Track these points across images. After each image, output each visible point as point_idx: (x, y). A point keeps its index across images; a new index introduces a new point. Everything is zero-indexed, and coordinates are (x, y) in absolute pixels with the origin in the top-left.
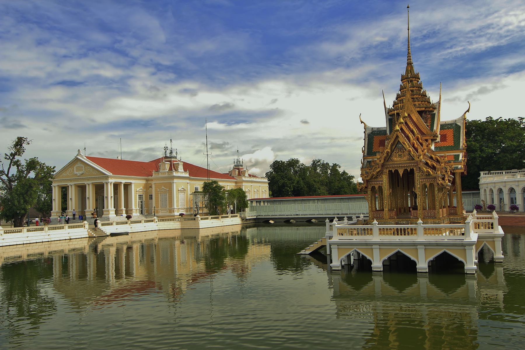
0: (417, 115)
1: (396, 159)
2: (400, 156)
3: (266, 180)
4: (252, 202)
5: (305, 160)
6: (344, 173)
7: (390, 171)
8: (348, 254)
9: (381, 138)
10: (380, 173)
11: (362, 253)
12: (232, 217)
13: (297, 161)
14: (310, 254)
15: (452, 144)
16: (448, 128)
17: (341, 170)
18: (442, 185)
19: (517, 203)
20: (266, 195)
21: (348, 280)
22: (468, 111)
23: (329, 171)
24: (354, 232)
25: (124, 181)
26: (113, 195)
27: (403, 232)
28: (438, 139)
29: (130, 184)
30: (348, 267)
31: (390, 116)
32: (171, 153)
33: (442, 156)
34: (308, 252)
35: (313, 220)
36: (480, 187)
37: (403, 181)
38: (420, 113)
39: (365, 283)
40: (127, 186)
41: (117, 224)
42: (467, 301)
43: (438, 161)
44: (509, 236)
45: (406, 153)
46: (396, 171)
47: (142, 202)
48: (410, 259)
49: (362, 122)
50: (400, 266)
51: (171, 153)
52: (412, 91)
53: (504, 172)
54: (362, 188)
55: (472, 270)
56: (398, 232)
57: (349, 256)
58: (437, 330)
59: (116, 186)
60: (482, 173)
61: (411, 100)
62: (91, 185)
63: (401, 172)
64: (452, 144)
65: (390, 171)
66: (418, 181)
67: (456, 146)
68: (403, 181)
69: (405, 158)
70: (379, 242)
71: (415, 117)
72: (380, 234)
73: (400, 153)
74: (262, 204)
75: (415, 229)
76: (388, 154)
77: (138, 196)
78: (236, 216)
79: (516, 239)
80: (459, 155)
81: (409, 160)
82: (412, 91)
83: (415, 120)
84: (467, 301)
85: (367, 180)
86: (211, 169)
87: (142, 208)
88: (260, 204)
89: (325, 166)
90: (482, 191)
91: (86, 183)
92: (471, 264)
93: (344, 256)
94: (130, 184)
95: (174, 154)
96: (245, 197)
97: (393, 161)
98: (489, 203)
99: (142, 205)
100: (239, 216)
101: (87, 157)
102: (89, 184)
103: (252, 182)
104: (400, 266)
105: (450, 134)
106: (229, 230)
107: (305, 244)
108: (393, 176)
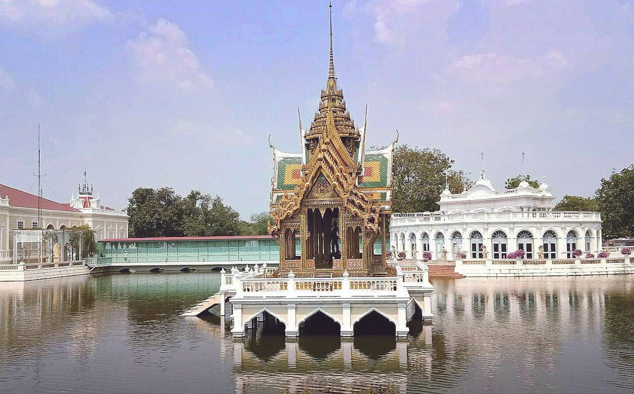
0: (340, 141)
3: (125, 214)
7: (310, 211)
8: (253, 316)
14: (198, 316)
15: (286, 182)
16: (374, 160)
18: (371, 229)
20: (126, 236)
21: (252, 347)
22: (396, 142)
24: (255, 285)
30: (252, 328)
31: (307, 140)
34: (197, 312)
37: (323, 225)
38: (343, 139)
39: (275, 352)
42: (394, 368)
45: (330, 188)
46: (317, 211)
48: (387, 320)
49: (271, 147)
50: (320, 330)
53: (416, 214)
54: (274, 231)
55: (402, 332)
57: (254, 320)
61: (333, 123)
65: (310, 211)
66: (343, 224)
68: (323, 225)
70: (293, 298)
71: (338, 143)
72: (352, 287)
74: (119, 247)
76: (308, 188)
80: (385, 193)
82: (334, 112)
83: (337, 146)
84: (394, 368)
85: (281, 220)
88: (116, 247)
92: (401, 327)
93: (249, 318)
98: (401, 250)
103: (106, 216)
104: (320, 330)
105: (375, 166)
107: (192, 300)
108: (313, 216)
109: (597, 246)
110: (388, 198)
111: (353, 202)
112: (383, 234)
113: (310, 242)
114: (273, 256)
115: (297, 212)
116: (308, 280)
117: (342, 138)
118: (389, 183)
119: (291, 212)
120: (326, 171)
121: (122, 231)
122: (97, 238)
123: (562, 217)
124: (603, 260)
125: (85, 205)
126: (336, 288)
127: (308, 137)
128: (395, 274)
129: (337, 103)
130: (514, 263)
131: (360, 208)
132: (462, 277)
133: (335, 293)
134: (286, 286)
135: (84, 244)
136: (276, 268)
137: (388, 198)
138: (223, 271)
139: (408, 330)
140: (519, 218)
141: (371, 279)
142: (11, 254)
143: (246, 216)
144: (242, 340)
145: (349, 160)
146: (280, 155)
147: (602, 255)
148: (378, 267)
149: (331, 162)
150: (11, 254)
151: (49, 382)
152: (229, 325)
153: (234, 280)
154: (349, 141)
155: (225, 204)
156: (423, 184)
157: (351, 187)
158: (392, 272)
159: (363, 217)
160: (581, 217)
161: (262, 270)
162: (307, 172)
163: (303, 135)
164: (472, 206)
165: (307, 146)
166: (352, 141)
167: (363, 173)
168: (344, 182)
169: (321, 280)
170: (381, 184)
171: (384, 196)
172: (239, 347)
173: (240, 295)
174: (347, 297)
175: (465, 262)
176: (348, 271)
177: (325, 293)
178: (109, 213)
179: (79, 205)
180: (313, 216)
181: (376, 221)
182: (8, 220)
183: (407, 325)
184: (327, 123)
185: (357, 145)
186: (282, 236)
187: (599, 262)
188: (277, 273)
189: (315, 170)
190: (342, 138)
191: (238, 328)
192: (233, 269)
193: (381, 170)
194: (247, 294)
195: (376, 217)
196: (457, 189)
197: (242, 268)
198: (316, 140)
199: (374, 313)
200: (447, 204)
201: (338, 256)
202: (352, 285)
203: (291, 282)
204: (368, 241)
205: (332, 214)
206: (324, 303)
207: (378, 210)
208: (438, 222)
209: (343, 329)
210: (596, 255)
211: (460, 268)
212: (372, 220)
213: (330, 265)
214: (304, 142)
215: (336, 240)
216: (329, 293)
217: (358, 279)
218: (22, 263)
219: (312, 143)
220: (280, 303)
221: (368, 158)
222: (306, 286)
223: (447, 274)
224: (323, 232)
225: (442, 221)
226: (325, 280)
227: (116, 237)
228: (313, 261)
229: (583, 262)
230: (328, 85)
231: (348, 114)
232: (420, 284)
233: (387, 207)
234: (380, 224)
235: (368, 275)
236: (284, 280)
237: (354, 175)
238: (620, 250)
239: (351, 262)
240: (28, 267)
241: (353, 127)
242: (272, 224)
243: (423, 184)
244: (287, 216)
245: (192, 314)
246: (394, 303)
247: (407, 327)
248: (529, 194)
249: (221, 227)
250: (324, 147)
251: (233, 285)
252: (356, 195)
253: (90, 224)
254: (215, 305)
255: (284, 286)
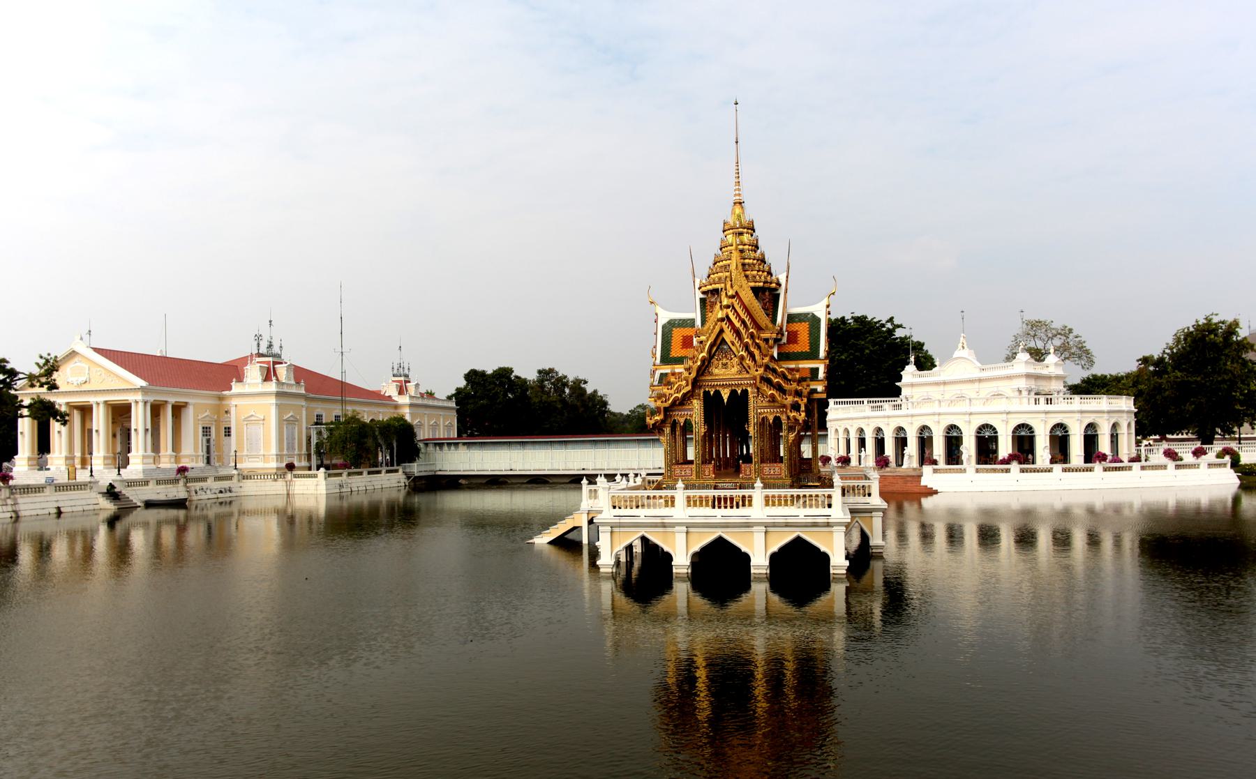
1: (717, 371)
2: (725, 365)
3: (453, 404)
4: (427, 445)
5: (527, 371)
6: (595, 391)
7: (706, 394)
9: (688, 331)
10: (686, 398)
11: (655, 539)
12: (388, 472)
13: (511, 371)
14: (550, 543)
15: (807, 349)
16: (801, 321)
17: (589, 390)
19: (887, 453)
23: (567, 391)
24: (628, 501)
25: (172, 400)
26: (149, 426)
27: (730, 502)
28: (785, 340)
29: (185, 405)
31: (703, 293)
32: (270, 346)
33: (792, 370)
35: (462, 481)
36: (828, 425)
37: (727, 415)
38: (756, 291)
40: (178, 410)
41: (158, 482)
43: (784, 377)
44: (893, 507)
45: (736, 360)
46: (718, 393)
47: (208, 441)
48: (818, 549)
50: (720, 568)
51: (270, 346)
52: (742, 251)
53: (866, 400)
56: (717, 502)
57: (629, 548)
58: (776, 663)
59: (156, 410)
60: (831, 401)
61: (740, 267)
62: (101, 406)
63: (725, 394)
64: (807, 349)
65: (706, 394)
67: (813, 355)
69: (735, 369)
70: (684, 525)
71: (747, 296)
73: (725, 361)
75: (750, 496)
77: (200, 430)
78: (396, 471)
79: (900, 509)
80: (817, 369)
81: (740, 372)
83: (746, 301)
86: (350, 380)
87: (208, 451)
89: (561, 382)
90: (831, 433)
91: (91, 399)
92: (839, 563)
93: (620, 547)
94: (185, 405)
95: (45, 355)
96: (413, 435)
97: (711, 374)
98: (843, 453)
99: (208, 448)
100: (401, 471)
101: (96, 350)
102: (98, 404)
104: (720, 568)
105: (803, 329)
106: (384, 498)
107: (548, 521)
108: (712, 403)
109: (1127, 446)
110: (821, 375)
111: (769, 381)
112: (816, 423)
113: (708, 439)
114: (652, 457)
115: (686, 398)
116: (704, 493)
117: (753, 289)
118: (822, 354)
119: (680, 395)
120: (729, 336)
121: (447, 425)
122: (422, 434)
123: (1078, 402)
124: (1136, 466)
125: (401, 392)
126: (744, 505)
127: (704, 289)
128: (831, 486)
129: (746, 238)
130: (1008, 471)
131: (779, 388)
132: (931, 492)
133: (742, 511)
134: (673, 502)
135: (400, 441)
136: (660, 478)
137: (821, 375)
138: (585, 481)
139: (847, 563)
140: (1015, 406)
141: (795, 492)
142: (309, 459)
143: (620, 404)
144: (614, 577)
145: (763, 319)
146: (665, 317)
147: (1137, 459)
148: (805, 474)
149: (738, 324)
150: (309, 459)
151: (962, 397)
152: (594, 554)
153: (601, 493)
154: (764, 293)
155: (589, 389)
156: (871, 358)
157: (766, 360)
158: (827, 483)
159: (786, 402)
160: (1102, 403)
161: (639, 480)
162: (703, 338)
163: (697, 286)
164: (948, 388)
165: (703, 301)
166: (768, 295)
167: (785, 340)
168: (756, 352)
169: (722, 493)
170: (813, 355)
171: (815, 371)
172: (607, 587)
173: (607, 515)
174: (760, 522)
175: (935, 471)
176: (762, 479)
177: (729, 512)
178: (431, 402)
179: (392, 391)
180: (712, 403)
181: (803, 408)
182: (304, 412)
183: (847, 558)
184: (733, 267)
185: (776, 298)
186: (667, 430)
187: (1130, 468)
188: (659, 482)
189: (713, 336)
190: (753, 289)
191: (606, 561)
192: (598, 479)
193: (810, 334)
194: (617, 512)
195: (803, 402)
196: (925, 363)
197: (611, 477)
198: (716, 292)
199: (799, 543)
200: (912, 385)
201: (748, 459)
202: (768, 501)
203: (680, 494)
204: (792, 436)
205: (740, 400)
206: (726, 526)
207: (805, 392)
208: (898, 412)
209: (754, 562)
210: (1125, 458)
211: (929, 478)
212: (796, 407)
213: (738, 471)
214: (699, 295)
215: (745, 438)
216: (735, 511)
217: (776, 492)
218: (322, 470)
219: (709, 298)
220: (664, 525)
221: (791, 318)
222: (701, 502)
223: (910, 487)
224: (725, 433)
225: (903, 411)
226: (728, 493)
227: (441, 434)
228: (711, 466)
229: (1210, 465)
230: (733, 213)
231: (763, 255)
232: (867, 499)
233: (820, 388)
234: (809, 412)
235: (792, 487)
236: (669, 493)
237: (771, 342)
238: (1161, 451)
239: (769, 469)
240: (330, 475)
241: (770, 273)
242: (653, 413)
243: (871, 358)
244: (674, 401)
245: (542, 540)
246: (828, 525)
247: (540, 372)
248: (1031, 370)
249: (561, 410)
250: (725, 302)
251: (596, 502)
252: (774, 371)
253: (408, 418)
254: (574, 528)
255: (671, 502)
